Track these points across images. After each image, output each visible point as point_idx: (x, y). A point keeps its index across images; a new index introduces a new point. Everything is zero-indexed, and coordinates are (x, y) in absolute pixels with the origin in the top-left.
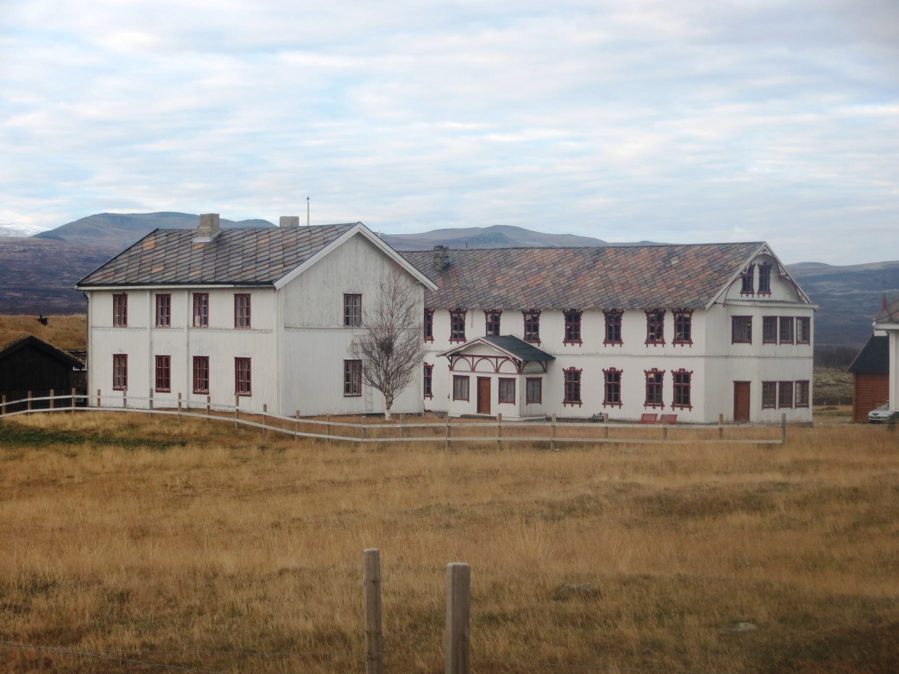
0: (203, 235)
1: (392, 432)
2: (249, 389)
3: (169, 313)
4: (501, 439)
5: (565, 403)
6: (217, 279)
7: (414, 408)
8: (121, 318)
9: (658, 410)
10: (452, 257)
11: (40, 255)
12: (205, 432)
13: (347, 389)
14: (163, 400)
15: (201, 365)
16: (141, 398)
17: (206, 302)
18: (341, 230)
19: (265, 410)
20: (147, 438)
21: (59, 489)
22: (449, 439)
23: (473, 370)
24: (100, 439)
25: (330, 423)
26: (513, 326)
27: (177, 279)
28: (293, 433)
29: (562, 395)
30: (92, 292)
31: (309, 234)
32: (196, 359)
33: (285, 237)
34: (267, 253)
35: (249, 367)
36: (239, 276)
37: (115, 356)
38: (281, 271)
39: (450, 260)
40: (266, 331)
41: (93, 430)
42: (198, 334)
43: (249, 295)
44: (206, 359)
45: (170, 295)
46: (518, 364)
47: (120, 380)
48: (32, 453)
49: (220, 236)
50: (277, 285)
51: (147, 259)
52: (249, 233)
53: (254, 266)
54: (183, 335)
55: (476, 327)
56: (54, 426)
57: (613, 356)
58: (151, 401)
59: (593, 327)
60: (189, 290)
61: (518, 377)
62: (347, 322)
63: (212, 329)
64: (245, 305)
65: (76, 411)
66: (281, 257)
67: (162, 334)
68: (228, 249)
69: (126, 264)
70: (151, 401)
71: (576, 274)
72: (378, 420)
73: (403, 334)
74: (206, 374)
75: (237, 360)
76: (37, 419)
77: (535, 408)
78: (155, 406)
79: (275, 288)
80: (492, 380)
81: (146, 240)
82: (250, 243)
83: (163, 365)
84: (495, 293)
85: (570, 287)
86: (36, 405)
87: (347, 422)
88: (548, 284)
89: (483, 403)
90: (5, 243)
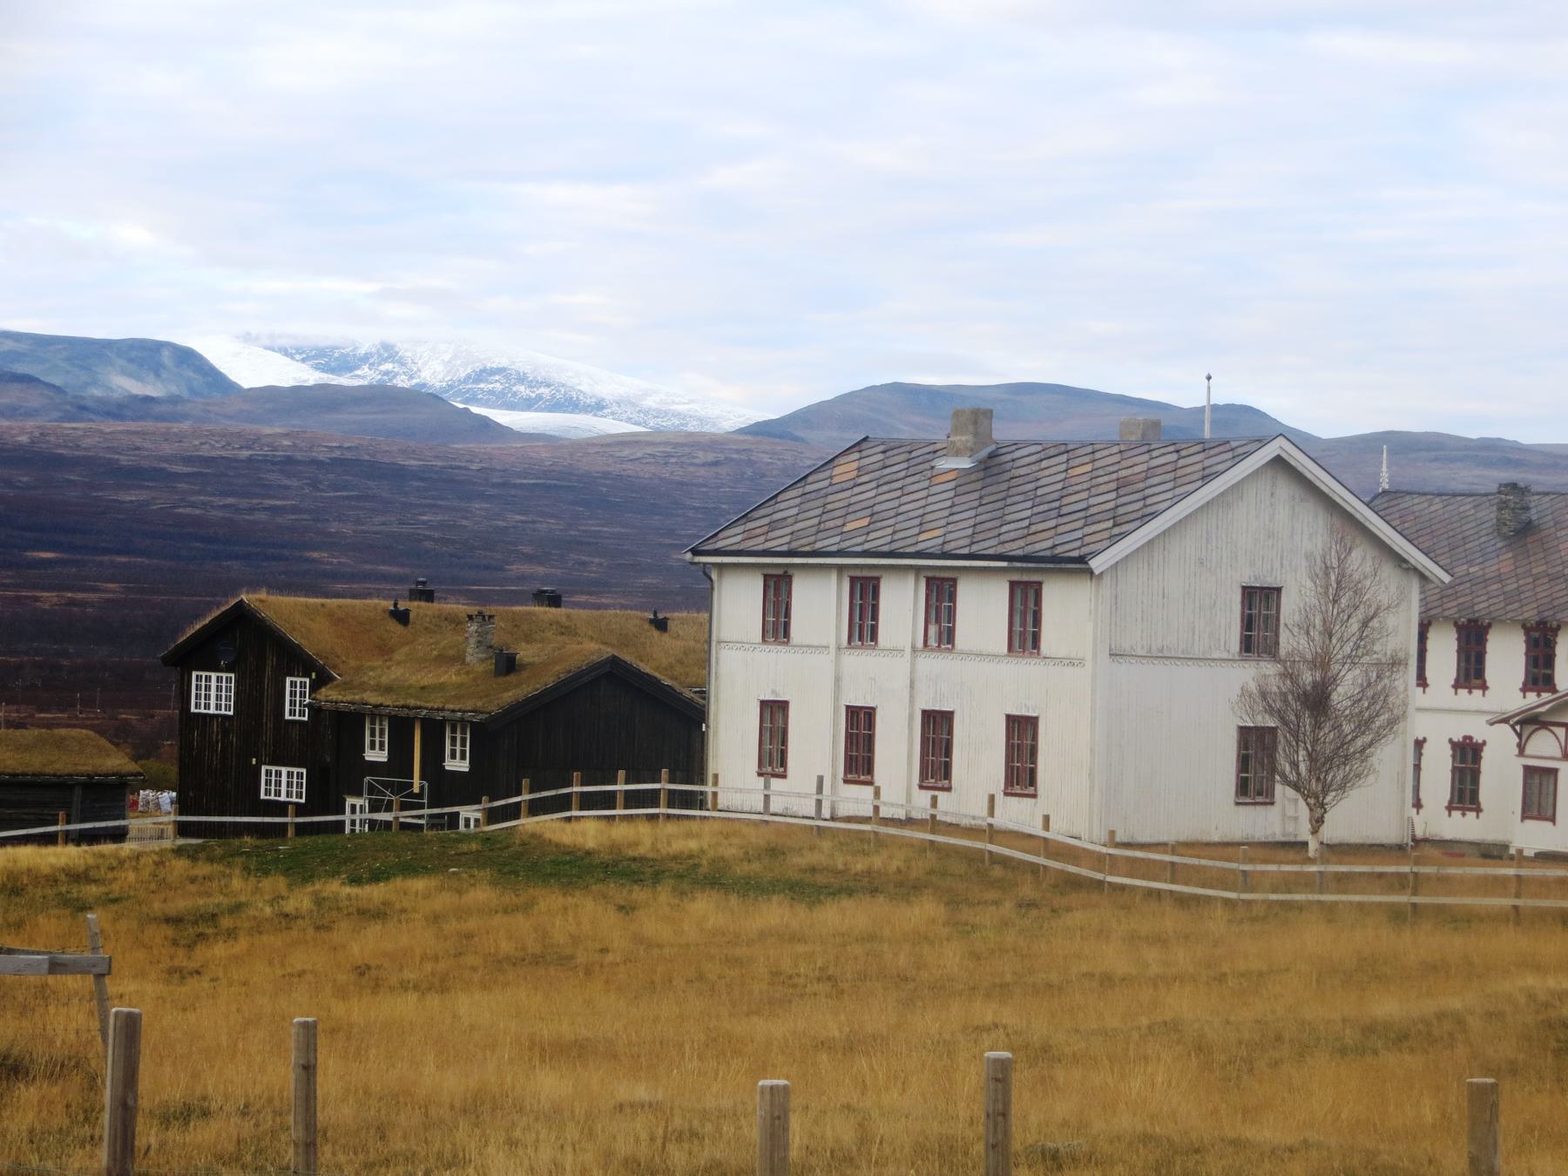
0: (958, 453)
1: (1307, 882)
2: (1032, 781)
3: (875, 617)
4: (1519, 902)
6: (974, 548)
7: (1388, 832)
8: (777, 626)
10: (1538, 510)
11: (749, 472)
12: (917, 871)
13: (1243, 788)
14: (855, 800)
15: (937, 729)
16: (799, 795)
17: (952, 597)
18: (1240, 451)
19: (1046, 827)
20: (796, 876)
22: (1416, 900)
24: (694, 876)
25: (1176, 859)
27: (894, 546)
28: (1099, 876)
30: (721, 567)
31: (1174, 457)
32: (928, 716)
33: (1124, 464)
34: (1084, 495)
35: (1035, 737)
36: (1021, 543)
37: (764, 704)
38: (1106, 534)
39: (1533, 515)
40: (1072, 662)
41: (691, 857)
42: (933, 664)
43: (1040, 584)
44: (948, 717)
45: (878, 579)
47: (774, 755)
48: (550, 900)
49: (992, 456)
50: (1096, 564)
51: (838, 500)
52: (1052, 452)
53: (1052, 523)
54: (902, 665)
56: (615, 847)
58: (767, 797)
60: (917, 570)
62: (1247, 645)
63: (961, 653)
64: (1031, 605)
65: (669, 816)
66: (1112, 505)
67: (859, 662)
68: (1005, 486)
69: (795, 511)
70: (767, 797)
72: (1291, 855)
73: (1349, 676)
75: (1012, 720)
76: (585, 830)
78: (772, 809)
79: (1091, 572)
81: (842, 460)
82: (1052, 475)
83: (860, 726)
86: (588, 802)
87: (1221, 859)
90: (676, 445)
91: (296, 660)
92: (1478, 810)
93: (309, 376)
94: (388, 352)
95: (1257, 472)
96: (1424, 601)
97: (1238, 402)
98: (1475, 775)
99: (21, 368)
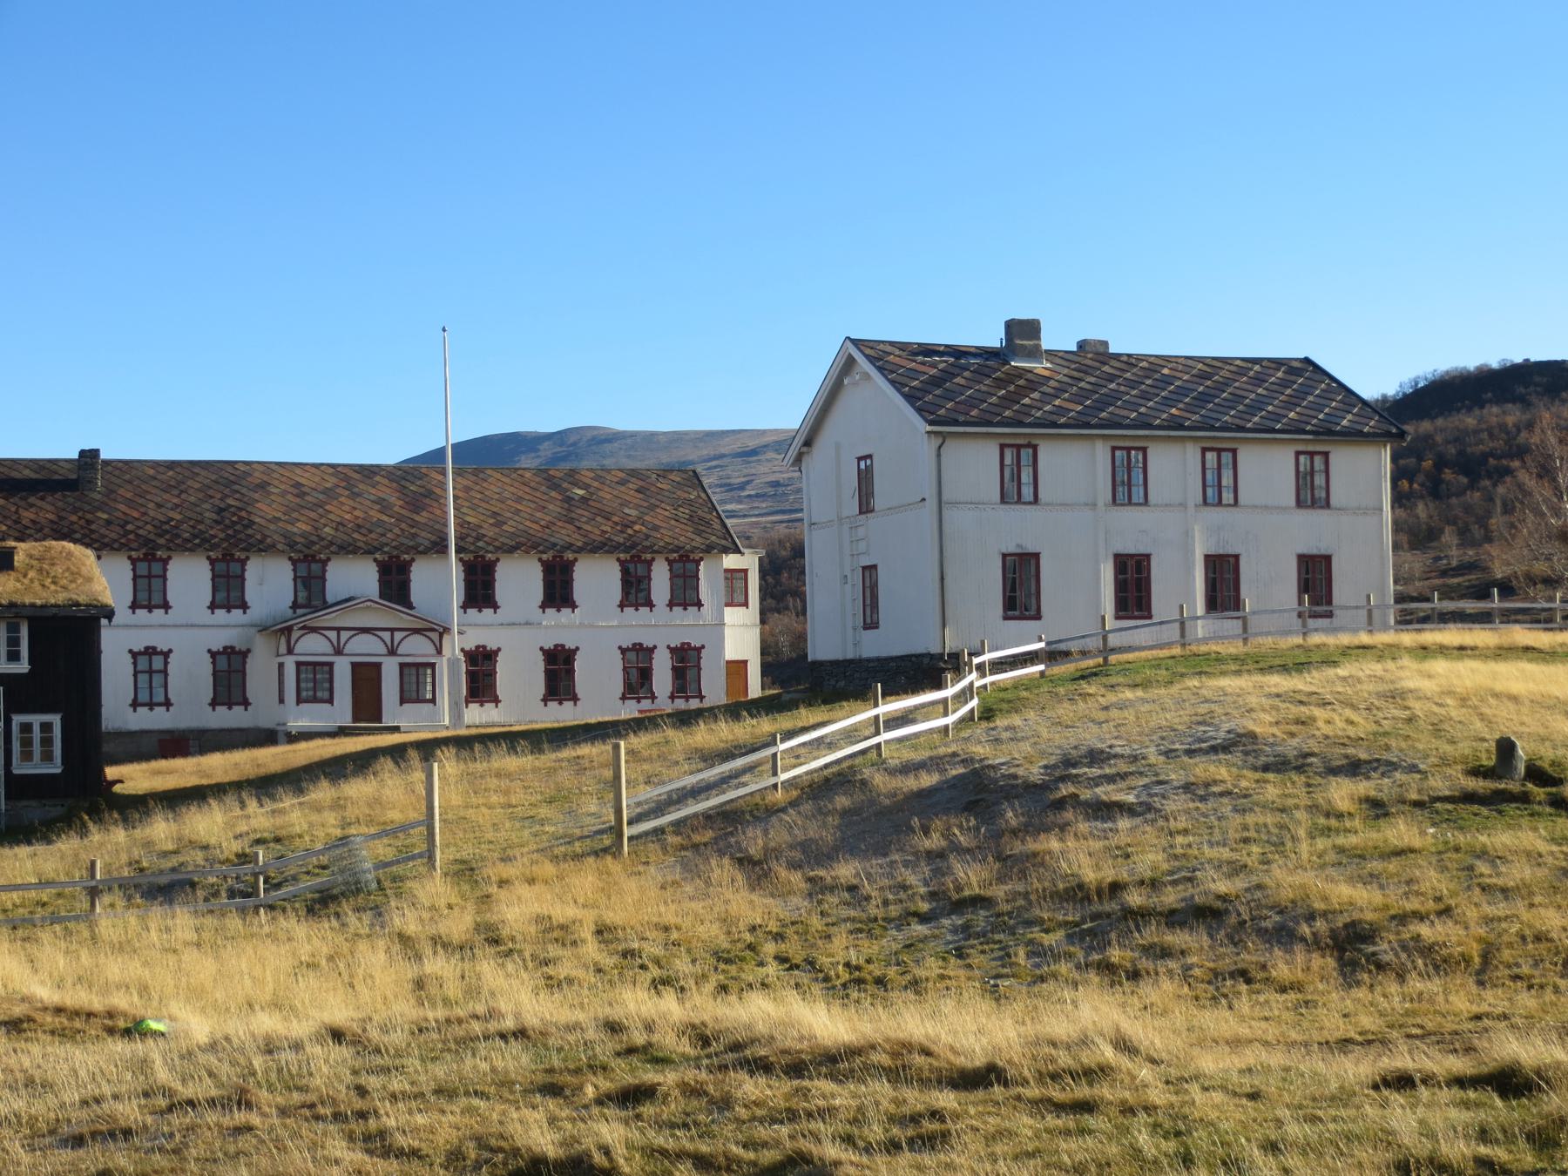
21: (1436, 1090)
57: (559, 627)
59: (519, 580)
80: (384, 668)
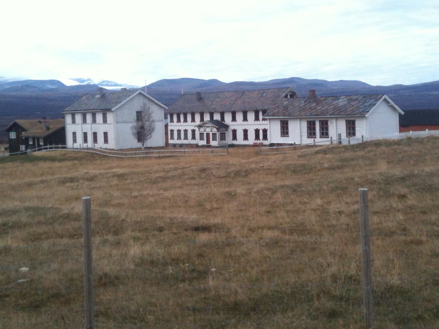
0: (98, 94)
5: (244, 140)
8: (74, 122)
9: (258, 142)
10: (202, 95)
14: (85, 145)
23: (205, 131)
26: (217, 117)
29: (231, 138)
32: (94, 133)
40: (110, 124)
42: (94, 125)
46: (217, 129)
47: (75, 141)
50: (113, 110)
54: (80, 126)
55: (207, 118)
59: (239, 116)
61: (217, 133)
67: (85, 126)
71: (236, 99)
74: (97, 138)
77: (224, 142)
84: (212, 107)
85: (234, 104)
88: (228, 103)
89: (208, 141)
91: (24, 130)
92: (248, 140)
93: (77, 83)
94: (89, 79)
95: (137, 95)
96: (165, 112)
97: (212, 79)
98: (195, 134)
99: (33, 85)
